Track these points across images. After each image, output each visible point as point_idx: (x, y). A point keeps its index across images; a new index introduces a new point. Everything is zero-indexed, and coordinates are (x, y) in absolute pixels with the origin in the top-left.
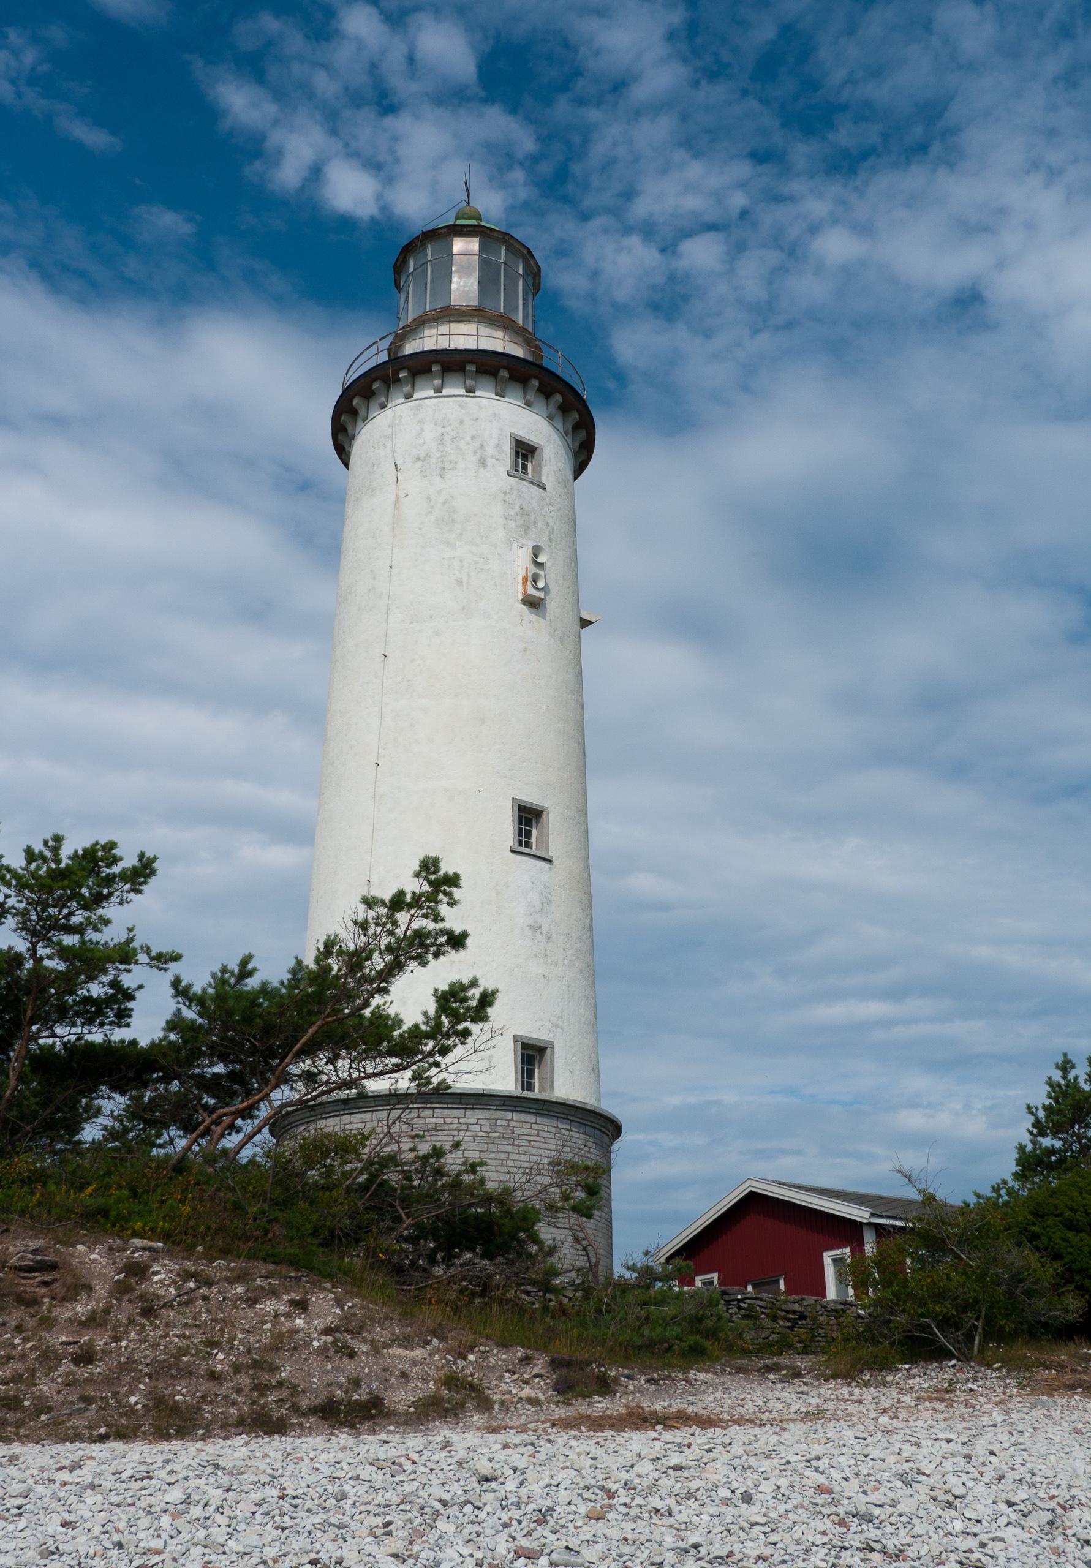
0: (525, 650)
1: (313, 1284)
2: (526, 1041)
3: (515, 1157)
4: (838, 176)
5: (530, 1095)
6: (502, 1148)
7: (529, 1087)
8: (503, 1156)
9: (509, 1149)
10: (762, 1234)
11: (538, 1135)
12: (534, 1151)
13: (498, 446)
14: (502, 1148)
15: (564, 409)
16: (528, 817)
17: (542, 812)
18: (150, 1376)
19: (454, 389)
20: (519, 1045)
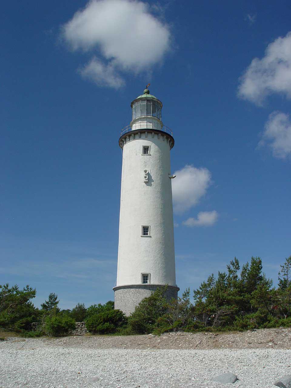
0: (145, 193)
1: (139, 316)
2: (143, 274)
3: (140, 296)
4: (125, 67)
5: (146, 284)
6: (137, 294)
7: (150, 283)
8: (137, 296)
9: (139, 294)
10: (80, 314)
11: (145, 291)
12: (143, 294)
13: (139, 150)
14: (137, 294)
15: (167, 138)
16: (145, 230)
17: (143, 227)
18: (153, 329)
19: (161, 138)
20: (142, 275)
